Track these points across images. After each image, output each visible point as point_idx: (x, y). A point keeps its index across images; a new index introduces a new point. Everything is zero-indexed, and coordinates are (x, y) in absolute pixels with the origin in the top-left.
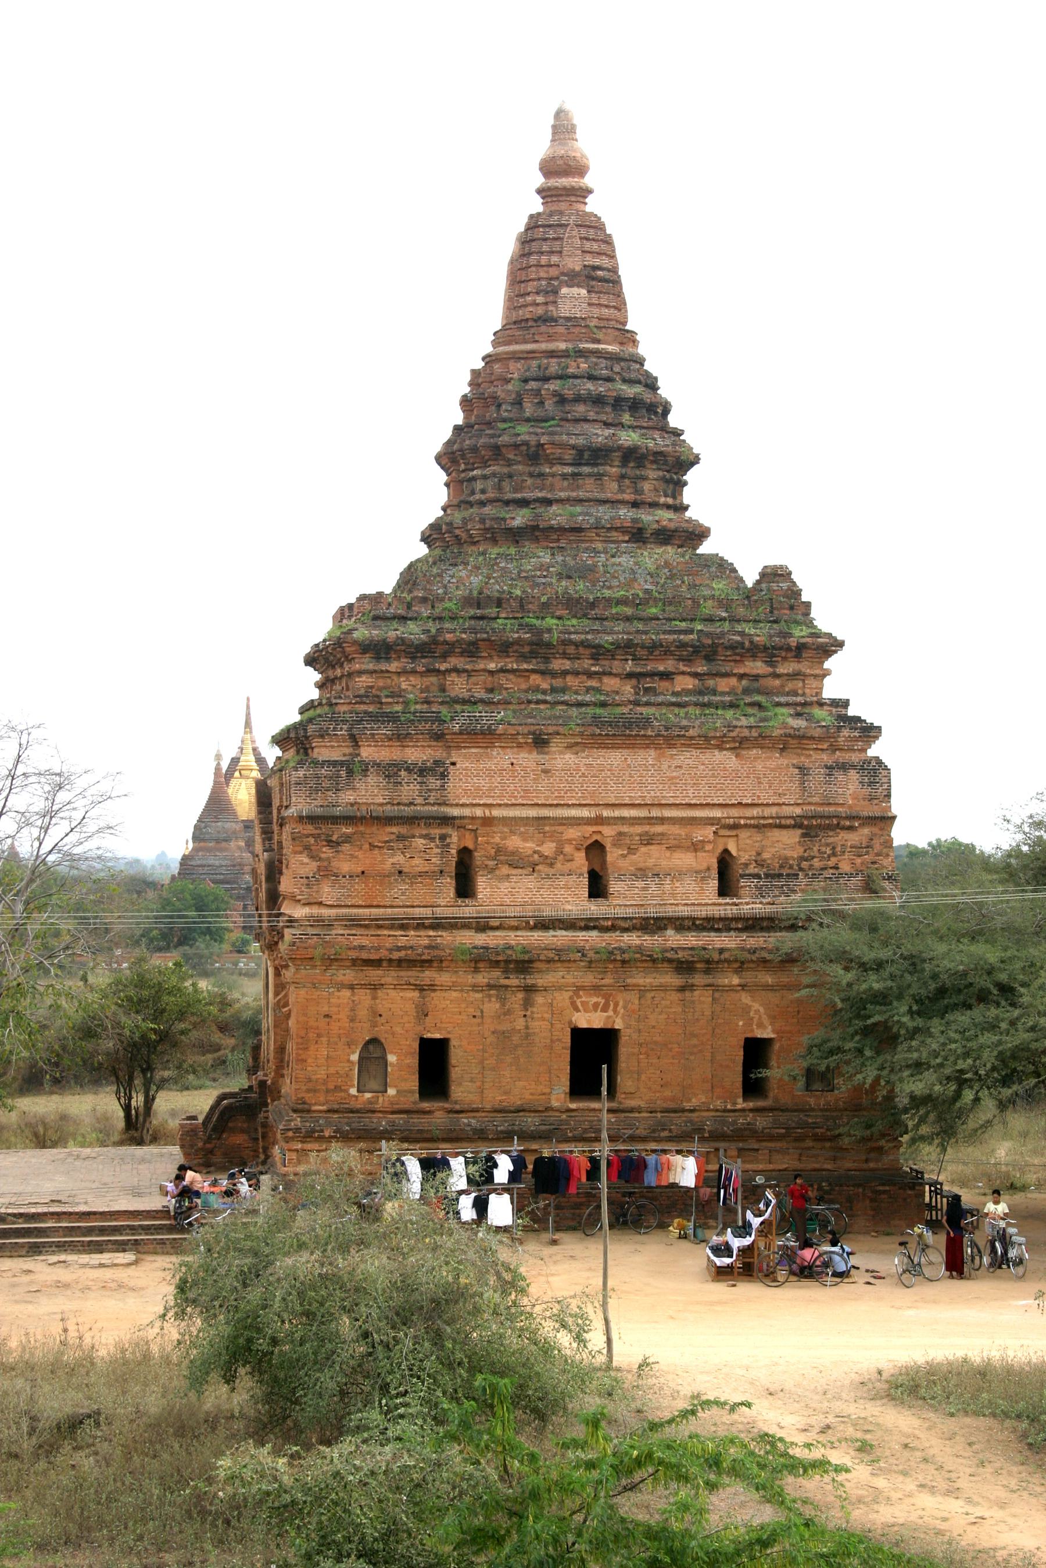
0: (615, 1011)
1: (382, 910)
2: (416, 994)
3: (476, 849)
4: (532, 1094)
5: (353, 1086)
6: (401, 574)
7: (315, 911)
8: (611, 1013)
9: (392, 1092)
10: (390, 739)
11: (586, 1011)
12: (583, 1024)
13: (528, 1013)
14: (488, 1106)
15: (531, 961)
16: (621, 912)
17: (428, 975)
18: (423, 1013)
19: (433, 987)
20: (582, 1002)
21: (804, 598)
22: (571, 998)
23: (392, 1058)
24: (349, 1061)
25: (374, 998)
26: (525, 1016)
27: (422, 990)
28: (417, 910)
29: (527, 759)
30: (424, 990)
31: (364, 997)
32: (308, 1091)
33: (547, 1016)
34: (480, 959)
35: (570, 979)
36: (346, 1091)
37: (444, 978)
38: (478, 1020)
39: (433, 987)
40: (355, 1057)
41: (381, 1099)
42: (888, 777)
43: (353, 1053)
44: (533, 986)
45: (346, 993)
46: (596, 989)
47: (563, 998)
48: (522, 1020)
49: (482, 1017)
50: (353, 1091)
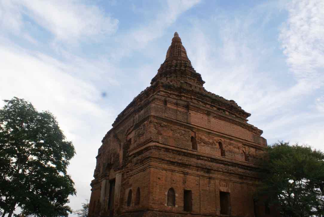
0: (229, 187)
1: (180, 149)
2: (183, 175)
3: (195, 137)
4: (212, 210)
5: (166, 203)
6: (159, 70)
7: (157, 144)
8: (228, 188)
9: (176, 206)
10: (174, 104)
11: (223, 186)
12: (222, 191)
13: (210, 186)
14: (202, 213)
15: (211, 170)
16: (226, 160)
17: (186, 170)
18: (184, 182)
19: (187, 174)
20: (222, 184)
21: (236, 103)
22: (219, 182)
23: (177, 195)
24: (165, 194)
25: (172, 175)
26: (209, 186)
27: (184, 174)
28: (183, 150)
29: (205, 117)
30: (186, 174)
31: (169, 173)
32: (153, 203)
33: (214, 187)
34: (198, 168)
35: (219, 176)
36: (164, 205)
37: (190, 171)
38: (198, 186)
39: (187, 174)
40: (166, 193)
41: (173, 208)
42: (266, 141)
43: (166, 191)
44: (211, 177)
45: (164, 172)
46: (224, 180)
47: (217, 181)
48: (208, 187)
49: (199, 185)
50: (166, 205)
